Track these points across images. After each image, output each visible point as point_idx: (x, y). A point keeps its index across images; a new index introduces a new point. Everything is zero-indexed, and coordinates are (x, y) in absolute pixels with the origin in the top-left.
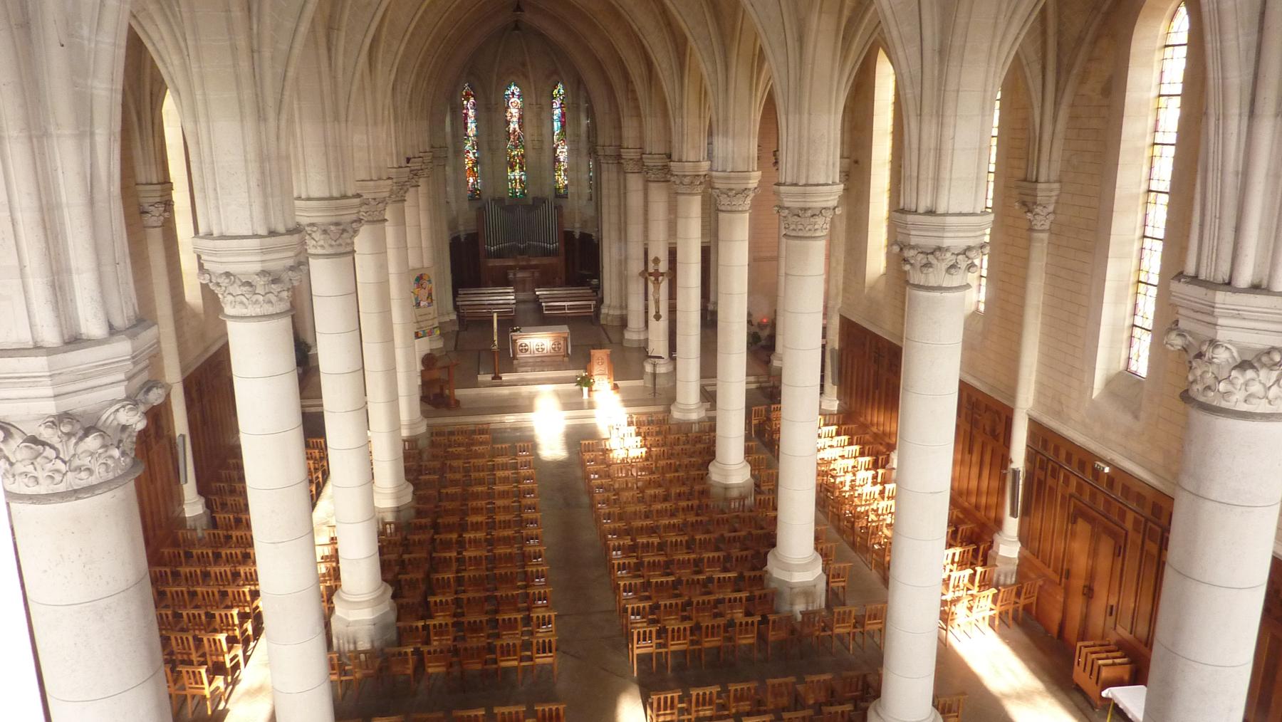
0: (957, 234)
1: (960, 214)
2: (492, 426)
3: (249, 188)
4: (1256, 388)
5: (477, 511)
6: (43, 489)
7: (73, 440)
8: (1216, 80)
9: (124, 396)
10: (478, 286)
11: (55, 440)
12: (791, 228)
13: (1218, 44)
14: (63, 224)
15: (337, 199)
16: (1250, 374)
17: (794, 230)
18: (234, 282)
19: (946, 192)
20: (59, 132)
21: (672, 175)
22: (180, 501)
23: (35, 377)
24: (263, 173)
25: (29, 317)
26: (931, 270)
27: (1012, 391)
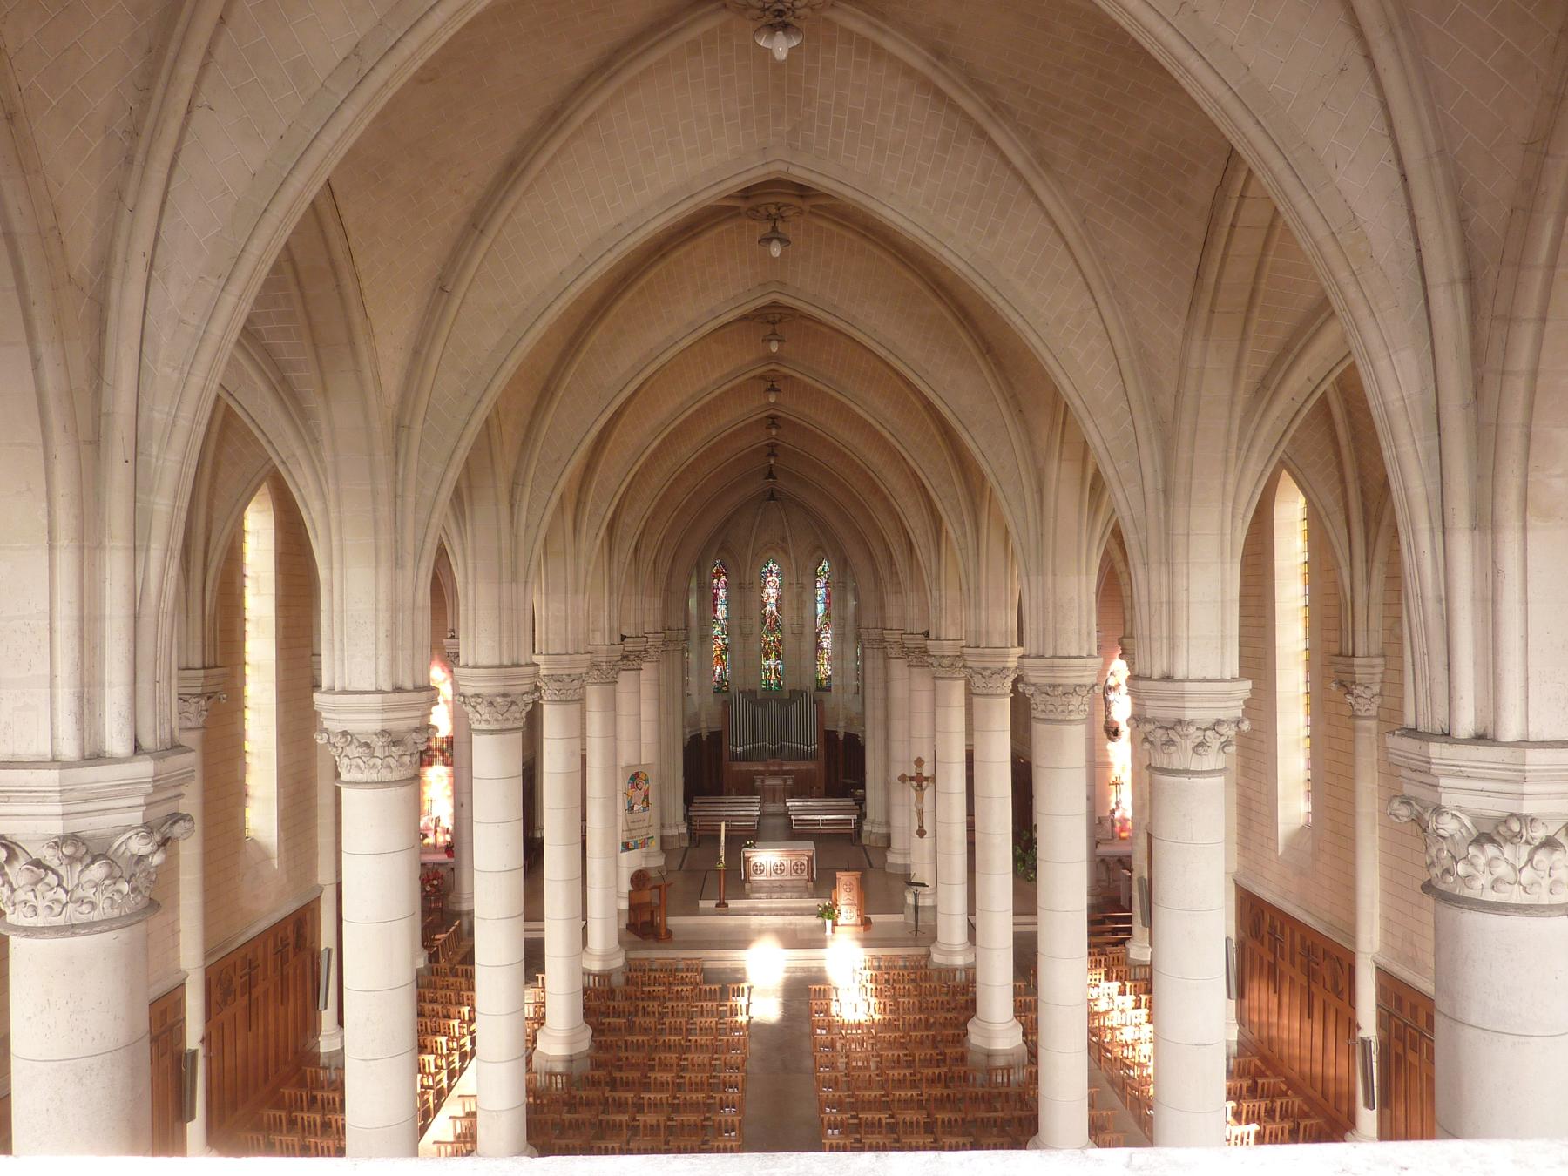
0: (1200, 705)
1: (1204, 680)
2: (708, 965)
3: (377, 638)
4: (1502, 870)
5: (665, 1067)
6: (39, 921)
7: (79, 867)
8: (1399, 492)
9: (140, 822)
10: (721, 794)
11: (54, 863)
12: (1040, 709)
13: (1394, 450)
14: (103, 637)
15: (507, 667)
16: (1491, 850)
17: (1043, 711)
18: (351, 742)
19: (1185, 654)
20: (111, 544)
21: (930, 656)
22: (316, 1030)
23: (45, 791)
24: (394, 623)
25: (52, 729)
26: (1173, 748)
27: (1351, 932)
